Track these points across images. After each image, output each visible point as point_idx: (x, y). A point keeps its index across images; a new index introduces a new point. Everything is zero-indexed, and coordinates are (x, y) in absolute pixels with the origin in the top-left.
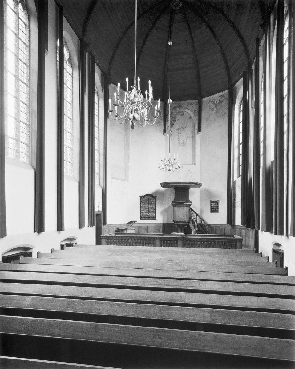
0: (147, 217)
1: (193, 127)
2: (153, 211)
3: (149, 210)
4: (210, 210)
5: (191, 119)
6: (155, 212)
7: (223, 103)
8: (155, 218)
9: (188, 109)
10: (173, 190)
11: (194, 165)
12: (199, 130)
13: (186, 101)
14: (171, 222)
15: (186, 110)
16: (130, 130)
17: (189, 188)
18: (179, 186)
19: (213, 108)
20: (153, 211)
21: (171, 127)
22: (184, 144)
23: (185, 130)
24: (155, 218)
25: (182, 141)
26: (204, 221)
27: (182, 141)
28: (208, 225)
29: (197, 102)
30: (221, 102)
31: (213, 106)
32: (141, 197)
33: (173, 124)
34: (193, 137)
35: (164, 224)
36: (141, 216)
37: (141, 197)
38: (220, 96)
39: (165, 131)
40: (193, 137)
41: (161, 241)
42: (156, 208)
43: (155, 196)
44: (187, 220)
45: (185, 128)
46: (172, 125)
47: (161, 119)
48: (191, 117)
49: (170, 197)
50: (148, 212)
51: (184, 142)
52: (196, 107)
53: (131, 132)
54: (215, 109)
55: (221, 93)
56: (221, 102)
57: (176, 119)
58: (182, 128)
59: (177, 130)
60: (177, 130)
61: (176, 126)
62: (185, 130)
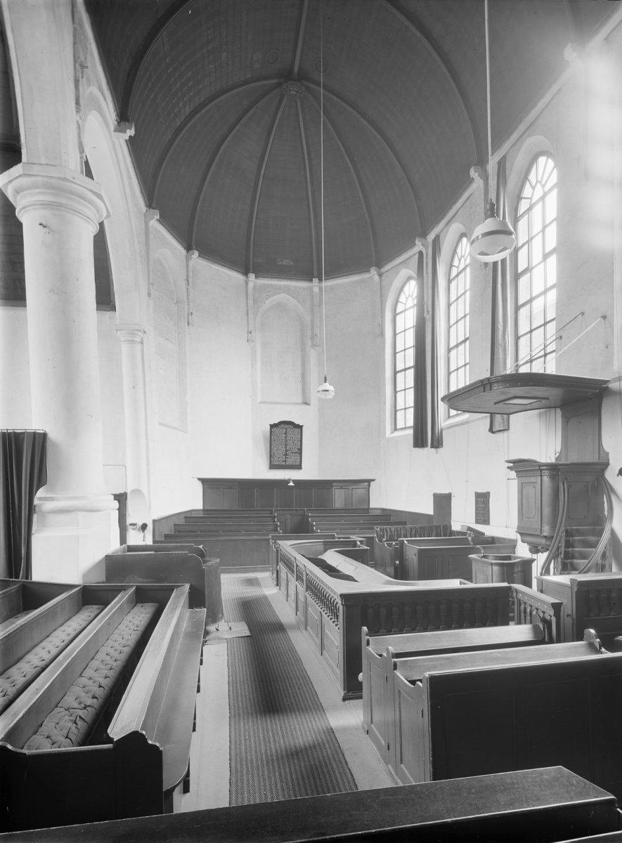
0: (284, 463)
2: (296, 453)
3: (286, 451)
4: (268, 466)
6: (301, 454)
20: (296, 453)
36: (271, 462)
37: (272, 426)
42: (301, 447)
50: (286, 455)
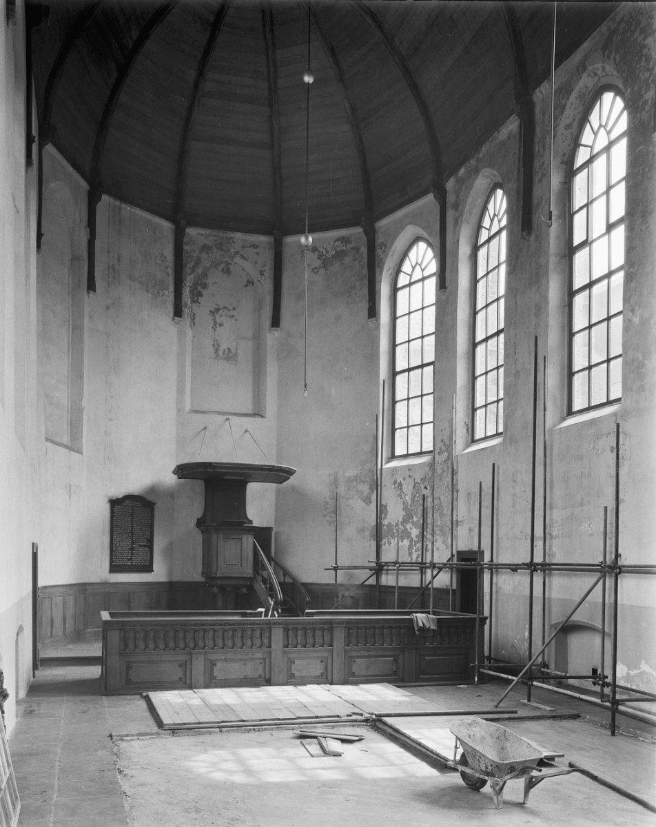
1: (258, 309)
2: (144, 546)
3: (133, 542)
5: (250, 288)
7: (347, 260)
8: (148, 568)
9: (243, 257)
10: (199, 485)
11: (258, 419)
12: (276, 322)
13: (239, 234)
14: (196, 575)
15: (238, 259)
16: (86, 291)
17: (247, 483)
18: (227, 474)
19: (315, 268)
21: (193, 301)
22: (230, 356)
23: (233, 316)
24: (148, 568)
25: (224, 346)
26: (293, 578)
27: (224, 346)
28: (304, 585)
29: (269, 243)
30: (340, 255)
31: (318, 263)
32: (114, 503)
33: (200, 295)
34: (258, 339)
35: (81, 589)
37: (114, 503)
38: (338, 240)
39: (178, 313)
40: (258, 339)
41: (286, 630)
43: (153, 502)
44: (249, 571)
45: (234, 309)
46: (196, 295)
47: (168, 275)
48: (250, 283)
49: (192, 507)
51: (229, 349)
52: (267, 256)
53: (89, 301)
54: (322, 271)
55: (343, 232)
56: (340, 255)
57: (210, 281)
58: (225, 308)
59: (211, 312)
60: (211, 312)
61: (206, 303)
62: (233, 316)
